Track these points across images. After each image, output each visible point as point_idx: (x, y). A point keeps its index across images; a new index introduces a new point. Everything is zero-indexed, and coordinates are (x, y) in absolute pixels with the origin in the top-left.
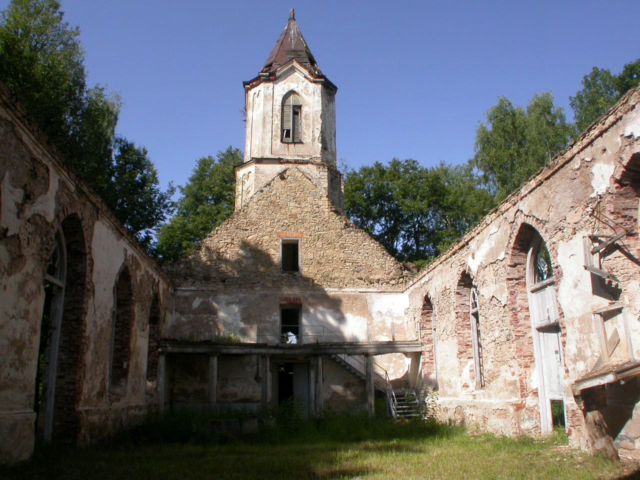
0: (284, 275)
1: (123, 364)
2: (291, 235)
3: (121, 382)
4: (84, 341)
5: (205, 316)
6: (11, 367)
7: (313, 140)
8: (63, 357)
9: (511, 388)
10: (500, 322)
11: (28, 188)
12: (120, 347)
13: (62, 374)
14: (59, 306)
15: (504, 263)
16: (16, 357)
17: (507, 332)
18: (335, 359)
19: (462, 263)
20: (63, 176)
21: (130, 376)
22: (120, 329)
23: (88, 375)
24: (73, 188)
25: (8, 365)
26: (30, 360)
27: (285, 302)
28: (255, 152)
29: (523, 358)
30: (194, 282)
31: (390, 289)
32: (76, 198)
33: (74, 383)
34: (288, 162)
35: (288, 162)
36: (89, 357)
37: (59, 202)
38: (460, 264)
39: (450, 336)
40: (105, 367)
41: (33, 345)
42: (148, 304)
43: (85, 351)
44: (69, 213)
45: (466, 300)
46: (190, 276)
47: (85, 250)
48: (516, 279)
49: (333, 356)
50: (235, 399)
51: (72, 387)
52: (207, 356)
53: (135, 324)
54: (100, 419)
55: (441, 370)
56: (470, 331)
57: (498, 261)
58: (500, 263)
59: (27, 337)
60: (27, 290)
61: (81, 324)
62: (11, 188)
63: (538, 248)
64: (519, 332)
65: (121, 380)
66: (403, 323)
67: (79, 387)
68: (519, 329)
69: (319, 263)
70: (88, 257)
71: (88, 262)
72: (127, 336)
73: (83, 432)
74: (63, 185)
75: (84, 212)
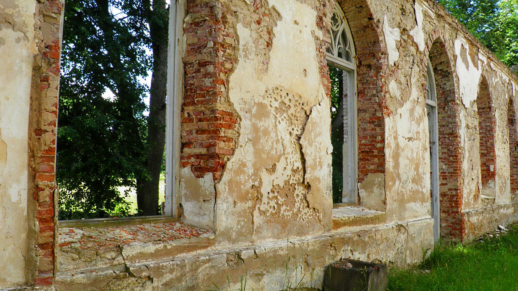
1: (490, 168)
3: (489, 184)
6: (413, 182)
8: (444, 167)
11: (402, 25)
13: (444, 182)
14: (351, 103)
16: (415, 173)
20: (424, 6)
21: (497, 177)
22: (483, 135)
23: (466, 181)
24: (433, 15)
32: (437, 24)
36: (465, 165)
37: (425, 30)
40: (477, 172)
41: (425, 161)
42: (505, 108)
43: (462, 159)
53: (497, 129)
54: (478, 220)
59: (421, 155)
60: (416, 115)
61: (457, 137)
62: (391, 29)
63: (40, 112)
65: (490, 181)
67: (460, 193)
70: (454, 74)
71: (455, 79)
72: (491, 141)
73: (467, 231)
74: (426, 15)
75: (446, 34)
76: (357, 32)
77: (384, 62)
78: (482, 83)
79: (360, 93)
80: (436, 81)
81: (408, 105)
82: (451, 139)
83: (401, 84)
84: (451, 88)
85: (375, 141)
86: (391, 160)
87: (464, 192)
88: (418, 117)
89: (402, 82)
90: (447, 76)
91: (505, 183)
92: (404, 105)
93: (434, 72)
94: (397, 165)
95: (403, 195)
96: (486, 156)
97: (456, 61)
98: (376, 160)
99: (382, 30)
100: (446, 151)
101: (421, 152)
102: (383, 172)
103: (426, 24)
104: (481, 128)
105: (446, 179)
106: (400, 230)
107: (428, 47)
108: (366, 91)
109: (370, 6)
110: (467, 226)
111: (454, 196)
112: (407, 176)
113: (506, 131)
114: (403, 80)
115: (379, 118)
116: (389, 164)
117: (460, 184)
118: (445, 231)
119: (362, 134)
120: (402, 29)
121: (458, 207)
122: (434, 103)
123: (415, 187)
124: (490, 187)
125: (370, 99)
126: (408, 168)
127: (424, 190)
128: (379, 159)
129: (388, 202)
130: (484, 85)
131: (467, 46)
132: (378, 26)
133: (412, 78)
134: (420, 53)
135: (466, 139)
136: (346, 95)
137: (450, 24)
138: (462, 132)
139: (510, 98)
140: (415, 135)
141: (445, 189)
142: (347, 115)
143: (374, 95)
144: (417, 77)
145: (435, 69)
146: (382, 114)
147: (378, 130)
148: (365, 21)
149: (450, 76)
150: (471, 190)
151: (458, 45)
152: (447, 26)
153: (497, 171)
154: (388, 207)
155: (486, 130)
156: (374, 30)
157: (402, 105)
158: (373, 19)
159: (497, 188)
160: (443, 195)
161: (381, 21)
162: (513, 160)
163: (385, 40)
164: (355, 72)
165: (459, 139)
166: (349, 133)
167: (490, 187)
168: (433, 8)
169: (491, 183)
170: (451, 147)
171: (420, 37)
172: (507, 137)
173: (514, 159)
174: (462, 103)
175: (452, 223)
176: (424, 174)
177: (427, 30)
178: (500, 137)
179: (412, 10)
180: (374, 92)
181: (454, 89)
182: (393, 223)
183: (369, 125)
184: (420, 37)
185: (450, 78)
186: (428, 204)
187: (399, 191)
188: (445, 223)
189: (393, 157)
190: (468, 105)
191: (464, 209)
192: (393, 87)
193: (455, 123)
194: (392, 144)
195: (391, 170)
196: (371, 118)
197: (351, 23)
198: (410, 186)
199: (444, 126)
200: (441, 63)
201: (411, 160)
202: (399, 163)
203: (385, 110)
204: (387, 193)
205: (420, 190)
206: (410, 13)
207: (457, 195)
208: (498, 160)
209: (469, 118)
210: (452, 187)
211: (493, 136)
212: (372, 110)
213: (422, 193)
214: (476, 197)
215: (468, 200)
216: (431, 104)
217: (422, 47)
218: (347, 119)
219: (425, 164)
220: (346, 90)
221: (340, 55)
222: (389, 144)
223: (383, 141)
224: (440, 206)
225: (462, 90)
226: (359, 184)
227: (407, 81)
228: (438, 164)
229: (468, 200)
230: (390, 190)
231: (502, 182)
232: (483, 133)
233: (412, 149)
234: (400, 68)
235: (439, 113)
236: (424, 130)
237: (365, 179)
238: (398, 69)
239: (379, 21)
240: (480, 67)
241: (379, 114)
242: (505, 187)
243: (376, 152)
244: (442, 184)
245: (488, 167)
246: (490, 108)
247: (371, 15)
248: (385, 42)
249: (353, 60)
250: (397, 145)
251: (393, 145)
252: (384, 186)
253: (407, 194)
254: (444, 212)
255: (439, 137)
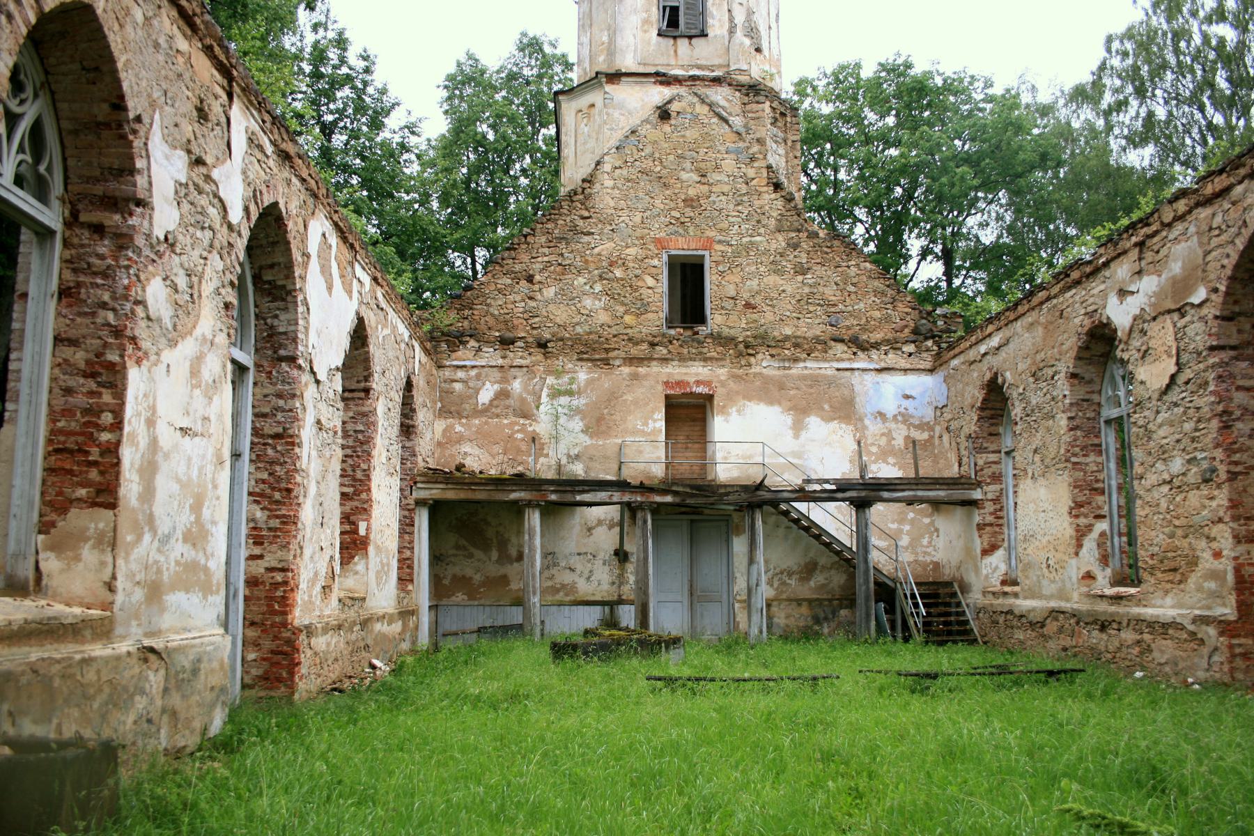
0: (672, 332)
2: (683, 246)
3: (356, 564)
4: (299, 479)
5: (506, 421)
6: (185, 540)
7: (732, 31)
8: (259, 514)
9: (1212, 585)
10: (1186, 441)
12: (350, 490)
13: (257, 551)
15: (1205, 311)
16: (192, 518)
17: (1205, 465)
18: (786, 514)
19: (1090, 309)
21: (371, 549)
22: (349, 452)
23: (307, 552)
25: (181, 537)
26: (214, 523)
27: (678, 391)
28: (601, 59)
29: (1242, 522)
30: (480, 349)
31: (903, 363)
33: (284, 570)
34: (677, 80)
35: (677, 80)
36: (307, 514)
37: (247, 177)
38: (1083, 311)
39: (1053, 469)
40: (333, 532)
42: (398, 398)
43: (301, 499)
44: (266, 204)
45: (1093, 392)
46: (471, 336)
47: (294, 284)
48: (1233, 348)
49: (783, 507)
50: (572, 598)
51: (279, 577)
52: (517, 509)
54: (328, 644)
55: (1025, 540)
56: (1099, 460)
57: (1188, 308)
58: (1193, 311)
59: (209, 476)
61: (293, 444)
64: (1236, 463)
65: (356, 558)
66: (932, 437)
68: (1237, 457)
69: (748, 305)
71: (301, 309)
75: (291, 199)
76: (76, 132)
77: (141, 225)
78: (355, 331)
79: (65, 293)
80: (256, 306)
81: (188, 347)
82: (279, 448)
83: (176, 291)
84: (292, 328)
85: (97, 426)
86: (135, 477)
87: (302, 577)
88: (210, 381)
89: (180, 289)
90: (284, 300)
91: (388, 565)
92: (179, 346)
93: (254, 284)
94: (148, 493)
95: (159, 571)
96: (351, 499)
97: (306, 268)
98: (94, 474)
99: (146, 144)
100: (265, 476)
101: (209, 468)
102: (113, 506)
103: (251, 163)
104: (346, 435)
105: (262, 544)
106: (146, 660)
107: (248, 218)
108: (83, 291)
109: (123, 75)
110: (305, 658)
111: (276, 585)
112: (171, 525)
113: (396, 448)
114: (182, 282)
115: (111, 366)
116: (130, 486)
117: (295, 556)
118: (254, 672)
119: (59, 402)
120: (194, 157)
121: (285, 613)
122: (246, 359)
123: (190, 553)
124: (356, 573)
125: (93, 314)
126: (176, 503)
127: (212, 565)
128: (102, 473)
129: (120, 584)
130: (359, 336)
131: (333, 240)
132: (135, 132)
133: (204, 282)
134: (230, 227)
135: (314, 453)
136: (24, 296)
137: (303, 180)
138: (307, 433)
139: (409, 377)
140: (199, 423)
141: (259, 568)
142: (20, 348)
143: (104, 305)
144: (216, 283)
145: (257, 278)
146: (122, 356)
147: (107, 397)
148: (102, 111)
149: (289, 298)
150: (316, 574)
151: (315, 235)
152: (294, 180)
153: (372, 537)
154: (120, 598)
155: (357, 440)
156: (123, 137)
157: (173, 343)
158: (125, 109)
159: (372, 575)
160: (252, 582)
161: (146, 120)
162: (405, 517)
163: (149, 169)
164: (59, 237)
165: (297, 450)
166: (24, 397)
167: (356, 573)
168: (271, 132)
169: (359, 564)
170: (278, 468)
171: (234, 193)
172: (396, 462)
173: (406, 513)
174: (311, 368)
175: (272, 652)
176: (214, 523)
177: (252, 177)
178: (384, 461)
179: (223, 120)
180: (106, 297)
181: (296, 332)
182: (131, 643)
183: (82, 381)
184: (234, 193)
185: (290, 306)
186: (219, 599)
187: (150, 561)
188: (254, 651)
189: (141, 471)
190: (322, 376)
191: (299, 617)
192: (156, 293)
193: (291, 410)
194: (140, 438)
195: (134, 502)
196: (88, 362)
197: (63, 106)
198: (179, 549)
199: (264, 415)
200: (272, 266)
201: (184, 485)
202: (154, 490)
203: (130, 349)
204: (120, 562)
205: (203, 562)
206: (217, 125)
207: (286, 583)
208: (376, 512)
209: (322, 406)
210: (274, 564)
211: (369, 455)
212: (94, 341)
213: (206, 569)
214: (326, 589)
215: (311, 596)
216: (240, 360)
217: (236, 215)
218: (20, 360)
219: (218, 498)
220: (27, 281)
221: (19, 181)
222: (133, 435)
223: (118, 425)
224: (245, 612)
225: (313, 338)
226: (41, 537)
227: (191, 287)
228: (245, 506)
229: (311, 596)
230: (128, 554)
231: (381, 562)
232: (348, 447)
233: (189, 459)
234: (178, 251)
235: (255, 384)
236: (220, 416)
237: (60, 524)
238: (173, 251)
239: (138, 119)
240: (355, 295)
241: (113, 357)
242: (387, 574)
243: (95, 454)
244: (252, 558)
245: (354, 524)
246: (367, 391)
247: (122, 97)
248: (150, 177)
249: (56, 204)
250: (154, 443)
251: (143, 441)
252: (111, 542)
253: (169, 569)
254: (253, 624)
255: (252, 443)
